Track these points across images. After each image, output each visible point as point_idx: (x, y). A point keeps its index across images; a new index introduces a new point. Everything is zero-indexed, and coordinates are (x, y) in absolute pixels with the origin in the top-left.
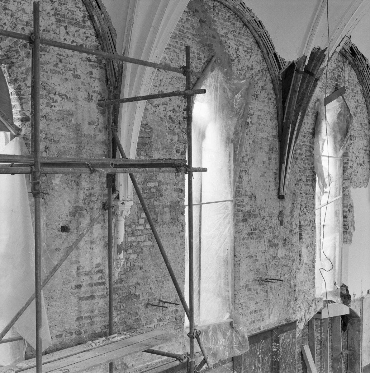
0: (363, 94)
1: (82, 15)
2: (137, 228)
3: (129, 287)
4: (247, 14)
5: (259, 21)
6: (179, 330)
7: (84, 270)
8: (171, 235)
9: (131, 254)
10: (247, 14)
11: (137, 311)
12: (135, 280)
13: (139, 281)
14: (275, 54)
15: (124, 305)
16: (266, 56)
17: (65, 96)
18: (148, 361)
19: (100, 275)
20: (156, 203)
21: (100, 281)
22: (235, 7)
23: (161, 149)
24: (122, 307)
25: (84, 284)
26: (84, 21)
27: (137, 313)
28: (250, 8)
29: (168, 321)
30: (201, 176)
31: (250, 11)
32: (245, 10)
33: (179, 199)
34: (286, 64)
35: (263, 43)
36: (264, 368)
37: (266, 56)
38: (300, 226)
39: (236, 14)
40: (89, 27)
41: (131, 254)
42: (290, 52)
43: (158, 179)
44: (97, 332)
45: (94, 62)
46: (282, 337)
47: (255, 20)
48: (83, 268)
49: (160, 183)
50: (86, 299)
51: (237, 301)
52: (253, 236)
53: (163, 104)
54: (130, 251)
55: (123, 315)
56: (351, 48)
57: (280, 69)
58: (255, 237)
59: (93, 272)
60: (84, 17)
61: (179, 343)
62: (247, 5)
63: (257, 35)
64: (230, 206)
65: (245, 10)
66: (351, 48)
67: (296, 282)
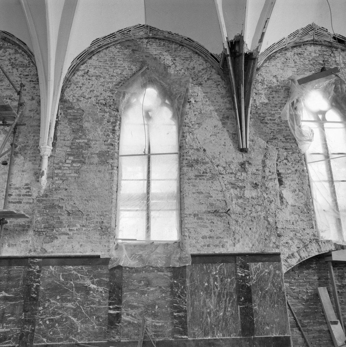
0: (264, 27)
1: (28, 62)
2: (64, 165)
3: (53, 200)
4: (177, 37)
5: (188, 38)
6: (105, 236)
7: (15, 186)
8: (99, 171)
9: (57, 180)
10: (177, 37)
11: (60, 216)
12: (60, 196)
13: (63, 197)
14: (211, 55)
15: (48, 211)
16: (206, 58)
17: (14, 99)
18: (68, 252)
19: (28, 190)
20: (84, 151)
21: (27, 194)
22: (165, 37)
23: (91, 121)
24: (45, 212)
25: (13, 194)
26: (29, 64)
27: (59, 218)
28: (177, 33)
29: (92, 228)
30: (337, 181)
31: (178, 35)
32: (174, 36)
33: (108, 150)
34: (220, 57)
35: (199, 51)
36: (226, 288)
37: (206, 58)
38: (279, 174)
39: (169, 41)
40: (32, 66)
41: (57, 180)
42: (218, 47)
43: (87, 138)
44: (21, 224)
45: (35, 81)
46: (253, 266)
47: (185, 39)
48: (14, 185)
49: (89, 140)
50: (14, 203)
51: (183, 226)
52: (204, 177)
53: (94, 97)
54: (56, 178)
55: (46, 217)
56: (334, 38)
57: (219, 62)
58: (205, 178)
59: (22, 188)
60: (29, 62)
61: (104, 246)
62: (173, 32)
63: (192, 48)
64: (176, 157)
65: (174, 36)
66: (334, 38)
67: (277, 220)
